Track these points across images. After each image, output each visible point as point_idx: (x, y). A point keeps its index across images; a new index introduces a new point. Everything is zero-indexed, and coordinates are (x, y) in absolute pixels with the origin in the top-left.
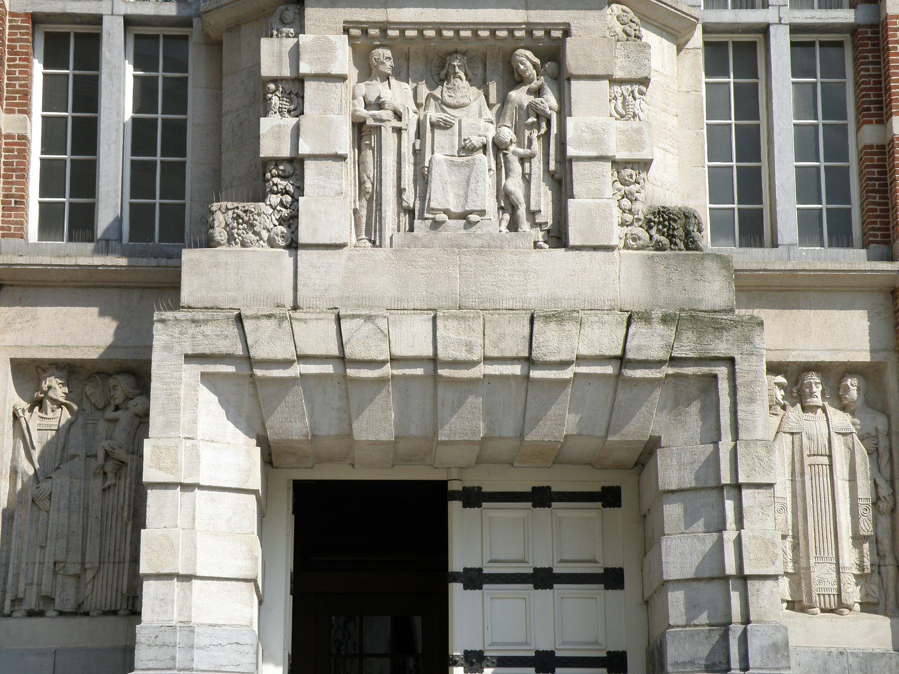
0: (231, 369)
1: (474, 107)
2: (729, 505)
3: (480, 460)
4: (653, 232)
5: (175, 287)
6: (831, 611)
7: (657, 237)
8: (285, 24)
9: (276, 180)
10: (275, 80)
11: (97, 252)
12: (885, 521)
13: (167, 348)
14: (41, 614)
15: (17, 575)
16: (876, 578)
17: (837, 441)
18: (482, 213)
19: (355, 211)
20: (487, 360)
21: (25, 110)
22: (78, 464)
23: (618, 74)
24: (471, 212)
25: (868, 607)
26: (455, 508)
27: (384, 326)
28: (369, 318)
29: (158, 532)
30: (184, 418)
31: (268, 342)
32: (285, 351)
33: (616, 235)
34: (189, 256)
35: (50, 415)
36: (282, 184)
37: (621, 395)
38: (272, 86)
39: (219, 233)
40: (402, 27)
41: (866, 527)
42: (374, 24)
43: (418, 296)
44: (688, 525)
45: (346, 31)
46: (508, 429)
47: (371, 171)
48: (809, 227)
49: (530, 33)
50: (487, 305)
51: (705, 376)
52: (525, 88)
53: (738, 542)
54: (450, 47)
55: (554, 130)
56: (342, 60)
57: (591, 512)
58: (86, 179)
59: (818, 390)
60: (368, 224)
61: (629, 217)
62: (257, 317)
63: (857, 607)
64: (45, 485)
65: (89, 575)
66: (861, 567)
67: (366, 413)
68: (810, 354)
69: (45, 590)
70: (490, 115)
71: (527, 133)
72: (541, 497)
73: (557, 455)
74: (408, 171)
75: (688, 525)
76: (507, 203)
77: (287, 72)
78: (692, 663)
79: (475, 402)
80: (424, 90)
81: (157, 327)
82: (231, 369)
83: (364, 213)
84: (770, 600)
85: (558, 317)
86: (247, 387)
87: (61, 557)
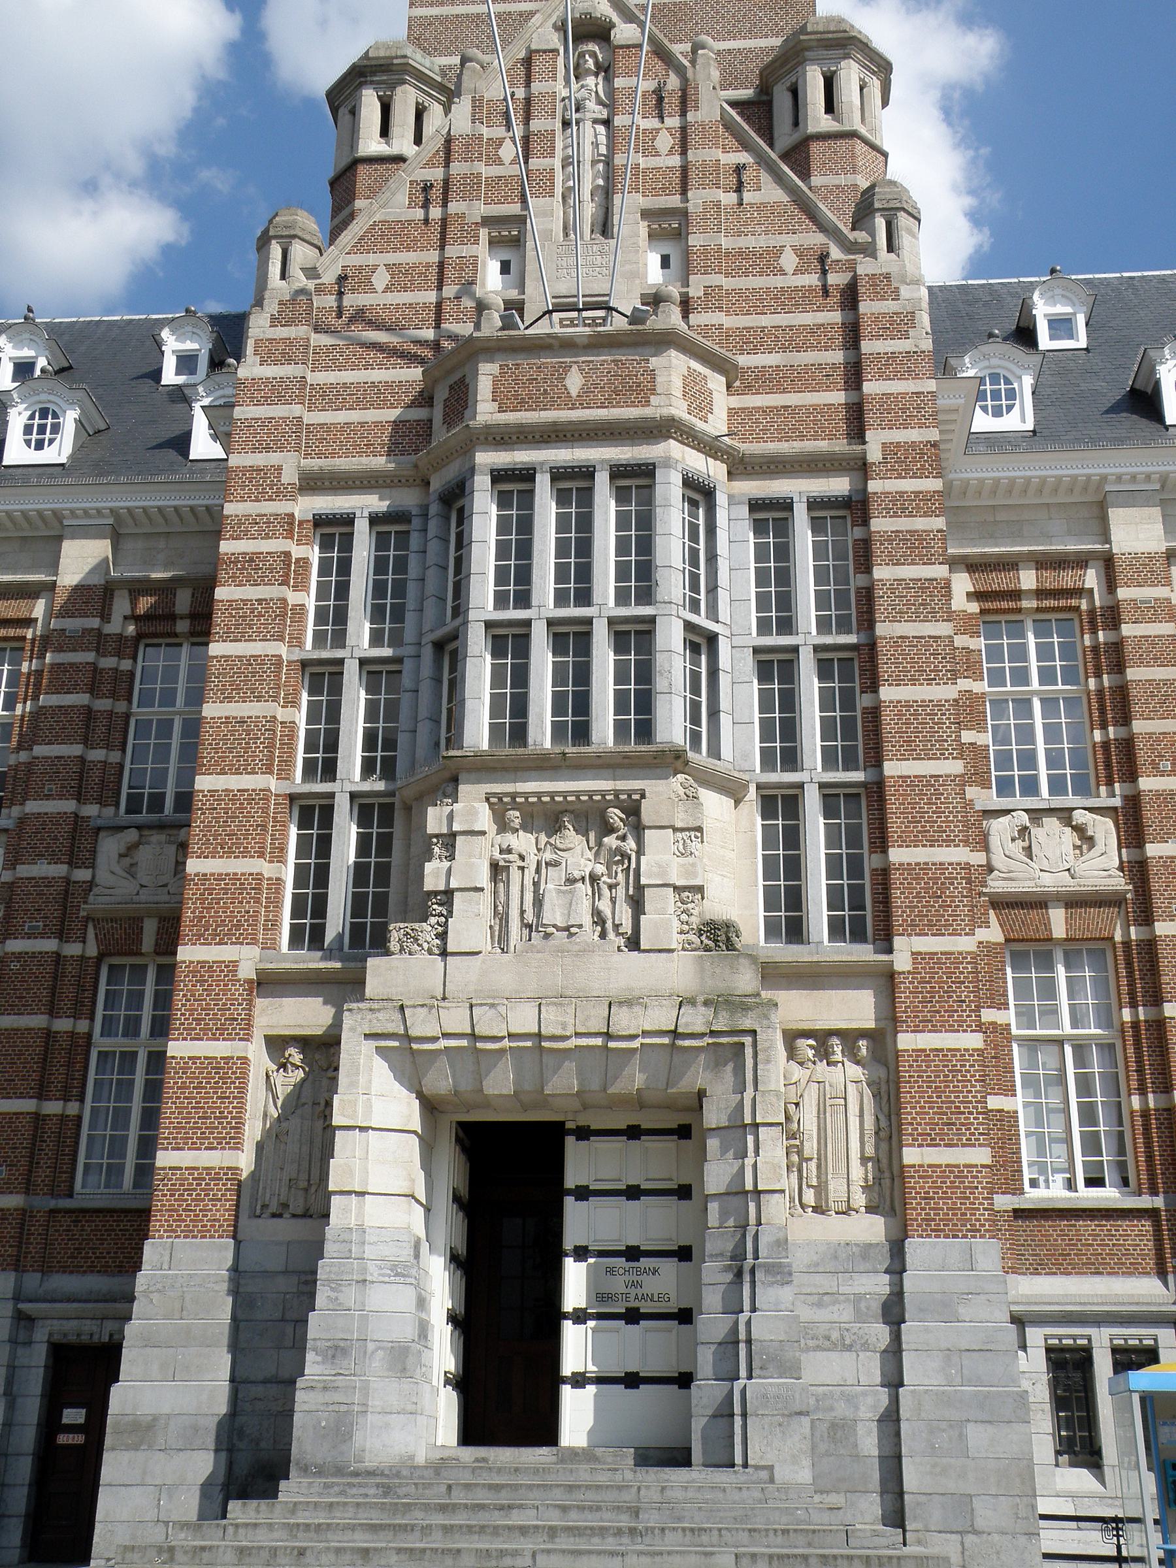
0: (396, 1044)
1: (578, 850)
2: (750, 1139)
3: (585, 1107)
4: (703, 938)
5: (362, 983)
6: (844, 1213)
7: (706, 941)
8: (446, 797)
9: (435, 907)
10: (437, 836)
11: (323, 959)
12: (884, 1146)
13: (353, 1029)
14: (280, 1216)
15: (265, 1188)
16: (876, 1188)
17: (851, 1088)
18: (580, 926)
19: (491, 927)
20: (578, 1035)
21: (282, 860)
22: (308, 1109)
23: (679, 825)
24: (572, 926)
25: (870, 1209)
26: (570, 1140)
27: (504, 1013)
28: (492, 1006)
29: (342, 1161)
30: (362, 1080)
31: (421, 1024)
32: (432, 1030)
33: (675, 941)
34: (371, 962)
35: (291, 1074)
36: (438, 909)
37: (675, 1058)
38: (435, 840)
39: (394, 945)
40: (527, 795)
41: (870, 1151)
42: (507, 794)
43: (531, 989)
44: (723, 1153)
45: (487, 799)
46: (595, 1085)
47: (502, 898)
48: (836, 929)
49: (617, 796)
50: (581, 994)
51: (736, 1043)
52: (615, 835)
53: (755, 1166)
54: (560, 808)
55: (633, 865)
56: (484, 818)
57: (669, 1144)
58: (320, 908)
59: (838, 1050)
60: (500, 936)
61: (686, 928)
62: (414, 1007)
63: (863, 1210)
64: (284, 1125)
65: (313, 1189)
66: (866, 1180)
67: (492, 1074)
68: (831, 1023)
69: (283, 1199)
70: (590, 855)
71: (615, 867)
72: (633, 1133)
73: (639, 1102)
74: (529, 897)
75: (723, 1153)
76: (599, 919)
77: (445, 831)
78: (722, 1255)
79: (570, 1066)
80: (543, 838)
81: (346, 1014)
82: (396, 1044)
83: (497, 928)
84: (776, 1209)
85: (628, 1003)
86: (407, 1057)
87: (294, 1176)
